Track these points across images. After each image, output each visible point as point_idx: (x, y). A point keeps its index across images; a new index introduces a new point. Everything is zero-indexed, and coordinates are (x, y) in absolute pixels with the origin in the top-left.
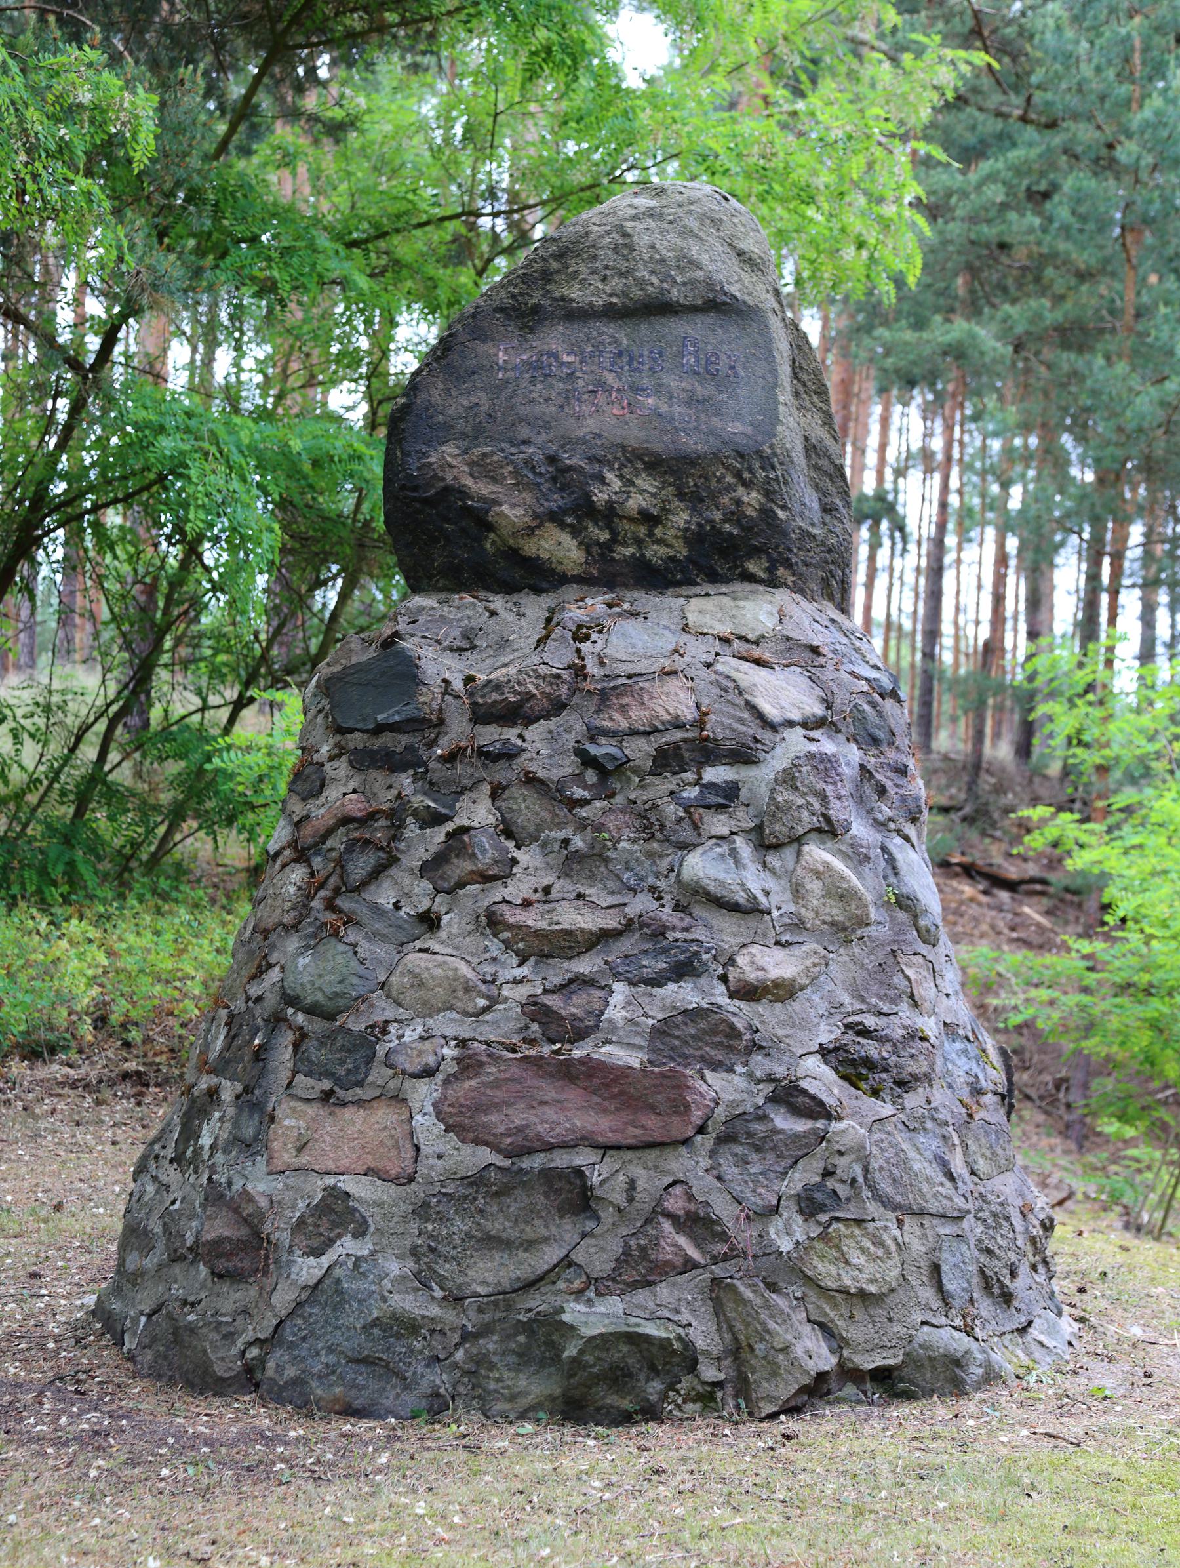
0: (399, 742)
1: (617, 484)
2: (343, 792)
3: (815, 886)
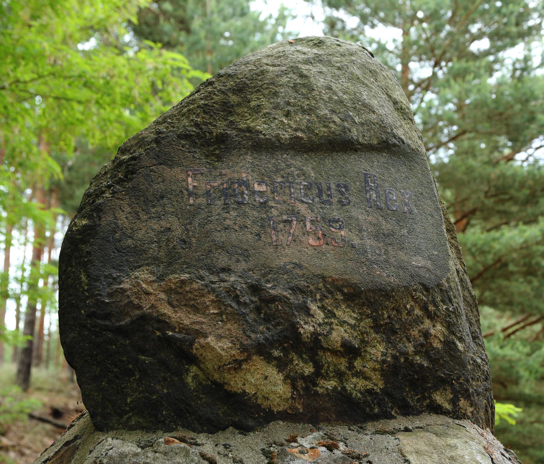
1: (320, 316)
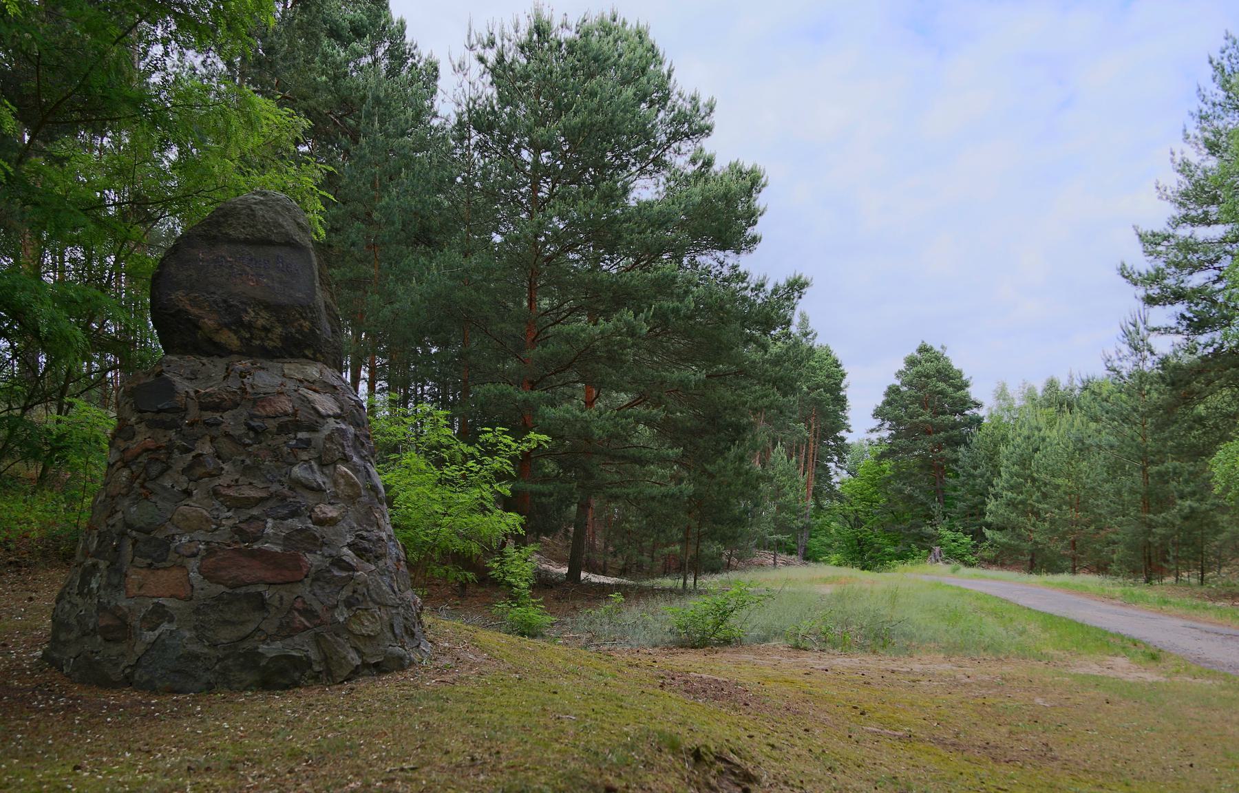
0: (168, 417)
1: (253, 314)
2: (143, 437)
3: (342, 481)
